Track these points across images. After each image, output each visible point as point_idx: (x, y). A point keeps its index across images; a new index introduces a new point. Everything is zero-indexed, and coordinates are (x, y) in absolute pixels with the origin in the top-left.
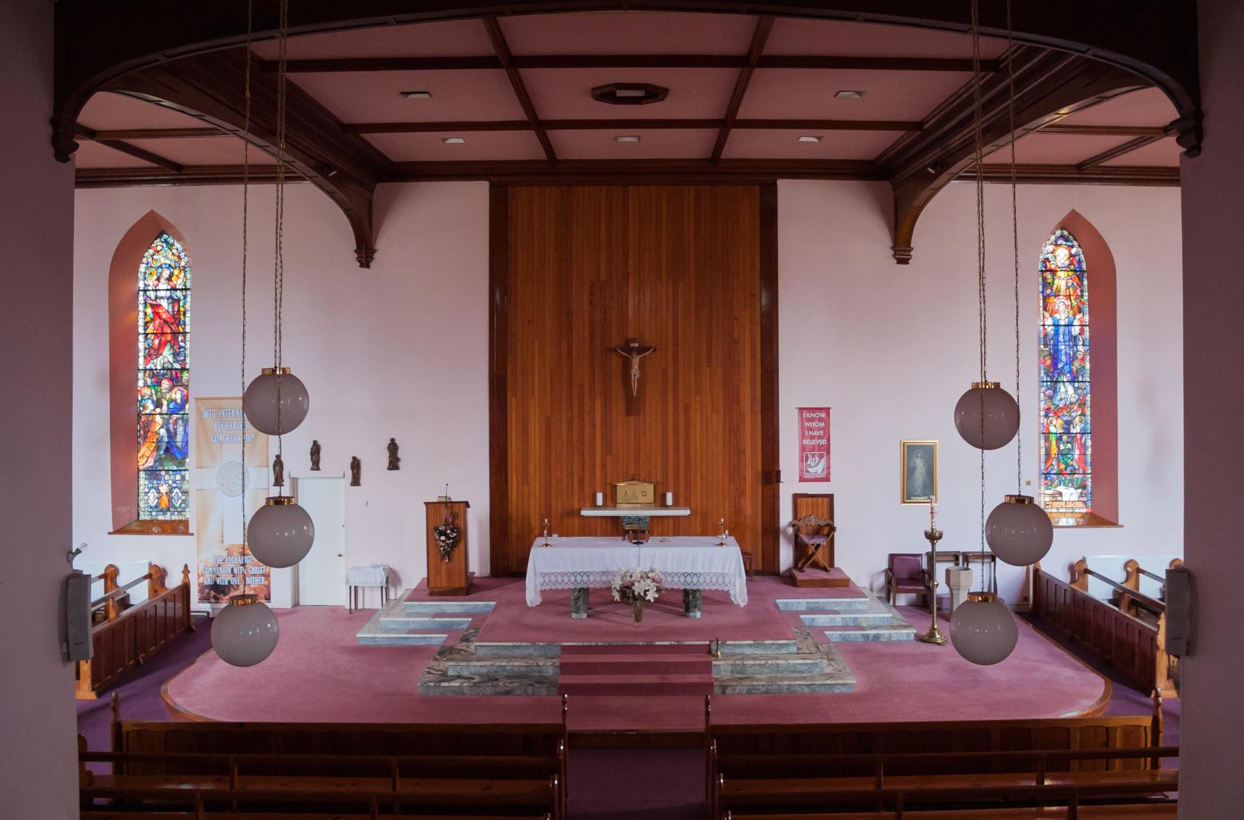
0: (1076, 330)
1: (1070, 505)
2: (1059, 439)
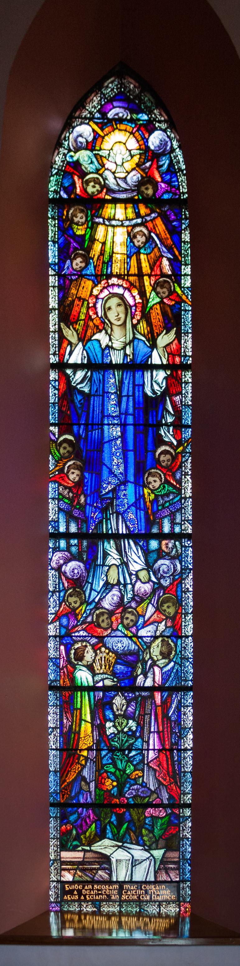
0: (155, 382)
1: (132, 893)
2: (101, 708)
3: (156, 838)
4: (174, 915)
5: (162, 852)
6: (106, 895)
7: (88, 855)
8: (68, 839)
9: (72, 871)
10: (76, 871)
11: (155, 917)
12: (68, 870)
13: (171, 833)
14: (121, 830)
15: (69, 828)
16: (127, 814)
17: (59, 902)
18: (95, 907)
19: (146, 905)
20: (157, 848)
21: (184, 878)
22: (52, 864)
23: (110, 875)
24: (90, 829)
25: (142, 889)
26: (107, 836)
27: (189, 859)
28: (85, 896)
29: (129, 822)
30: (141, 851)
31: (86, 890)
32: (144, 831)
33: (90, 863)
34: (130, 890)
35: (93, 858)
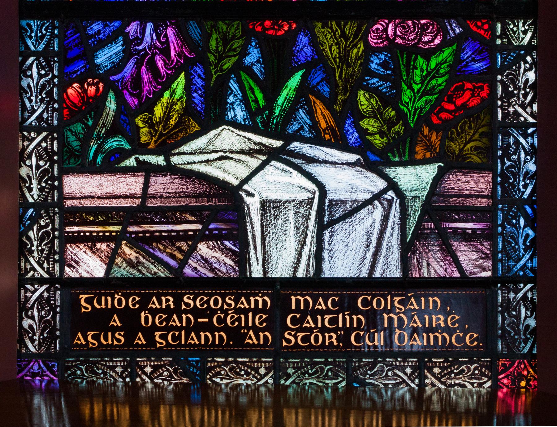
3: (406, 124)
4: (472, 402)
5: (428, 172)
6: (226, 329)
7: (159, 184)
8: (89, 131)
9: (102, 246)
10: (118, 246)
11: (404, 411)
12: (90, 241)
13: (464, 106)
14: (278, 94)
15: (91, 90)
16: (303, 40)
17: (56, 356)
18: (185, 374)
19: (374, 365)
20: (413, 162)
21: (509, 269)
22: (34, 220)
23: (242, 258)
24: (167, 95)
25: (357, 311)
26: (231, 114)
27: (529, 201)
28: (149, 333)
29: (309, 66)
30: (351, 171)
31: (154, 312)
32: (364, 101)
33: (167, 214)
34: (314, 313)
35: (178, 195)
